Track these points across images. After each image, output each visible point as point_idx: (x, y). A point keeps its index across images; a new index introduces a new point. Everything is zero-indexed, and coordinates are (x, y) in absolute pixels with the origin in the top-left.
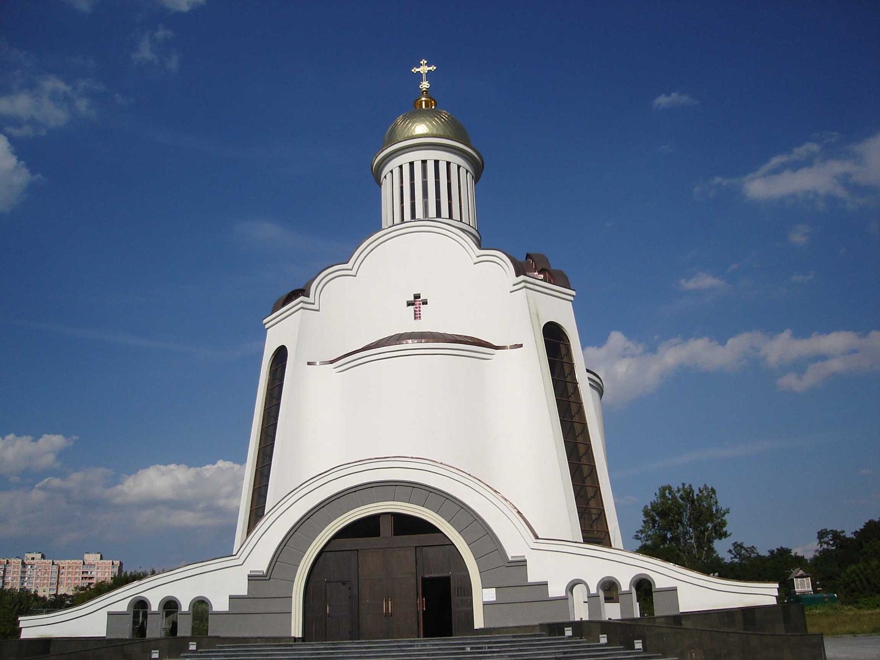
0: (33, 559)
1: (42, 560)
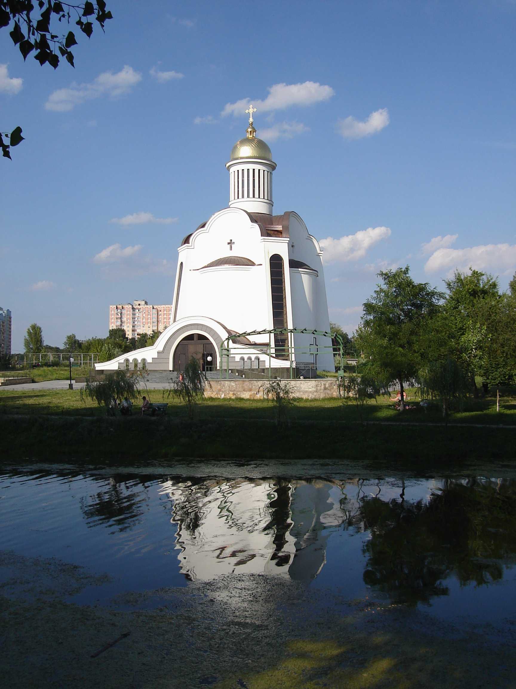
0: (139, 305)
1: (146, 306)
